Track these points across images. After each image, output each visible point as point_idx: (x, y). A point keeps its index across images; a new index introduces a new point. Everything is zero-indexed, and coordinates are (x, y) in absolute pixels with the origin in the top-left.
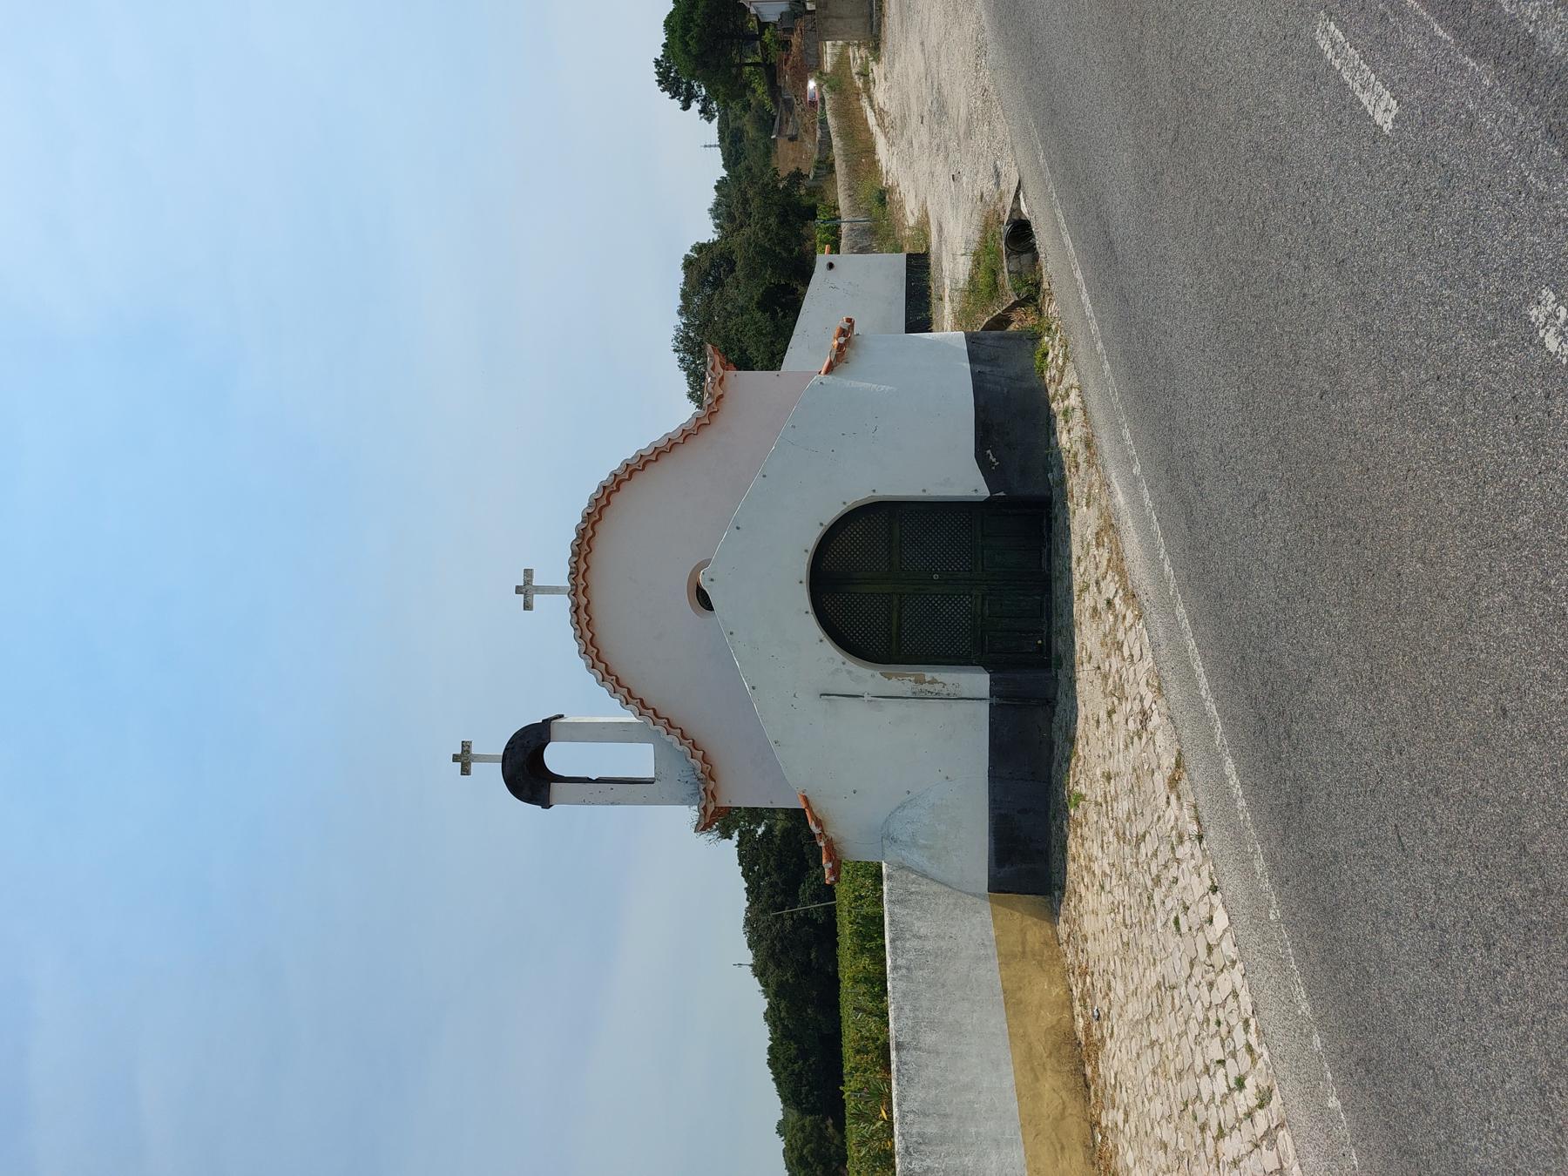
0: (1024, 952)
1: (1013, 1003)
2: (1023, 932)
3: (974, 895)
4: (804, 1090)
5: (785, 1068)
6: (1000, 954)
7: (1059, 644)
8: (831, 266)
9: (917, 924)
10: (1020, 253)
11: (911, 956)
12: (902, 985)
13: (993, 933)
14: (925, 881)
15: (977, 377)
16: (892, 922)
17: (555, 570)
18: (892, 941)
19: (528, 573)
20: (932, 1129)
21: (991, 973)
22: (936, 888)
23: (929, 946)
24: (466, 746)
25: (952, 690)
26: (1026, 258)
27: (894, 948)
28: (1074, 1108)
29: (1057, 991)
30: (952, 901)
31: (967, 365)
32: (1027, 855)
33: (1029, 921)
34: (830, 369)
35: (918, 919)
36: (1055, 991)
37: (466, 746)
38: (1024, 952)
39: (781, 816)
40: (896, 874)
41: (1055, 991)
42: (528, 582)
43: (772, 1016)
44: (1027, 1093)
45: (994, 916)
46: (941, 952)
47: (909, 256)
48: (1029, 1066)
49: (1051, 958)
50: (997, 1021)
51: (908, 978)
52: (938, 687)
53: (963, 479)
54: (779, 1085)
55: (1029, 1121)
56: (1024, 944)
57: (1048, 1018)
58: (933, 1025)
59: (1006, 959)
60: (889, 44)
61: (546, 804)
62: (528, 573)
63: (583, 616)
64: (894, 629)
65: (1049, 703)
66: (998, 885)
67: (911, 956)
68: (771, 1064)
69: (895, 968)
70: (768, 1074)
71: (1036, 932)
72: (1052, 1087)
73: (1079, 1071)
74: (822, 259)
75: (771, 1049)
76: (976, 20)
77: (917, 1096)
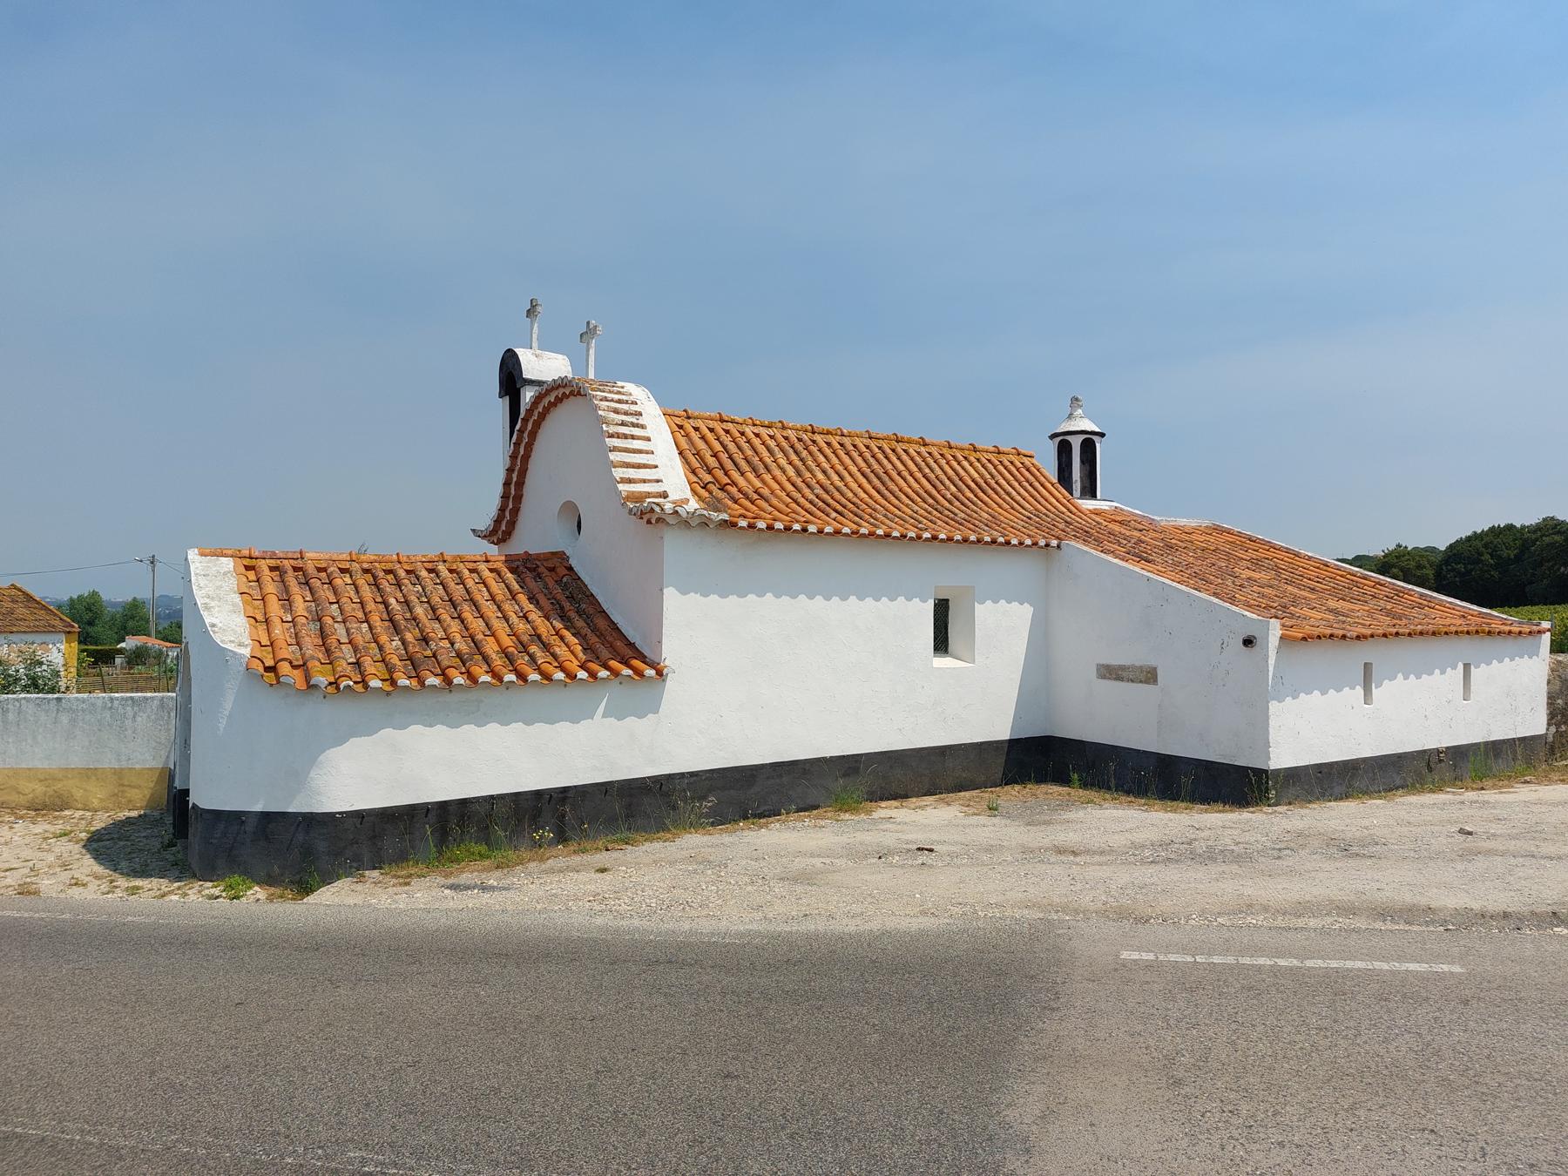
1: (88, 774)
2: (139, 787)
4: (1461, 567)
5: (1486, 546)
8: (1248, 642)
11: (121, 710)
12: (99, 703)
15: (237, 817)
16: (146, 698)
20: (11, 716)
21: (109, 762)
23: (128, 723)
27: (127, 699)
28: (22, 800)
29: (96, 803)
33: (147, 793)
34: (941, 644)
36: (96, 802)
41: (96, 802)
44: (32, 774)
48: (47, 778)
50: (77, 762)
51: (104, 707)
54: (1469, 539)
55: (16, 773)
57: (78, 794)
58: (73, 721)
59: (118, 773)
60: (1303, 811)
67: (121, 710)
68: (1492, 529)
69: (112, 699)
70: (1482, 526)
72: (37, 790)
73: (45, 807)
75: (1510, 527)
77: (30, 709)
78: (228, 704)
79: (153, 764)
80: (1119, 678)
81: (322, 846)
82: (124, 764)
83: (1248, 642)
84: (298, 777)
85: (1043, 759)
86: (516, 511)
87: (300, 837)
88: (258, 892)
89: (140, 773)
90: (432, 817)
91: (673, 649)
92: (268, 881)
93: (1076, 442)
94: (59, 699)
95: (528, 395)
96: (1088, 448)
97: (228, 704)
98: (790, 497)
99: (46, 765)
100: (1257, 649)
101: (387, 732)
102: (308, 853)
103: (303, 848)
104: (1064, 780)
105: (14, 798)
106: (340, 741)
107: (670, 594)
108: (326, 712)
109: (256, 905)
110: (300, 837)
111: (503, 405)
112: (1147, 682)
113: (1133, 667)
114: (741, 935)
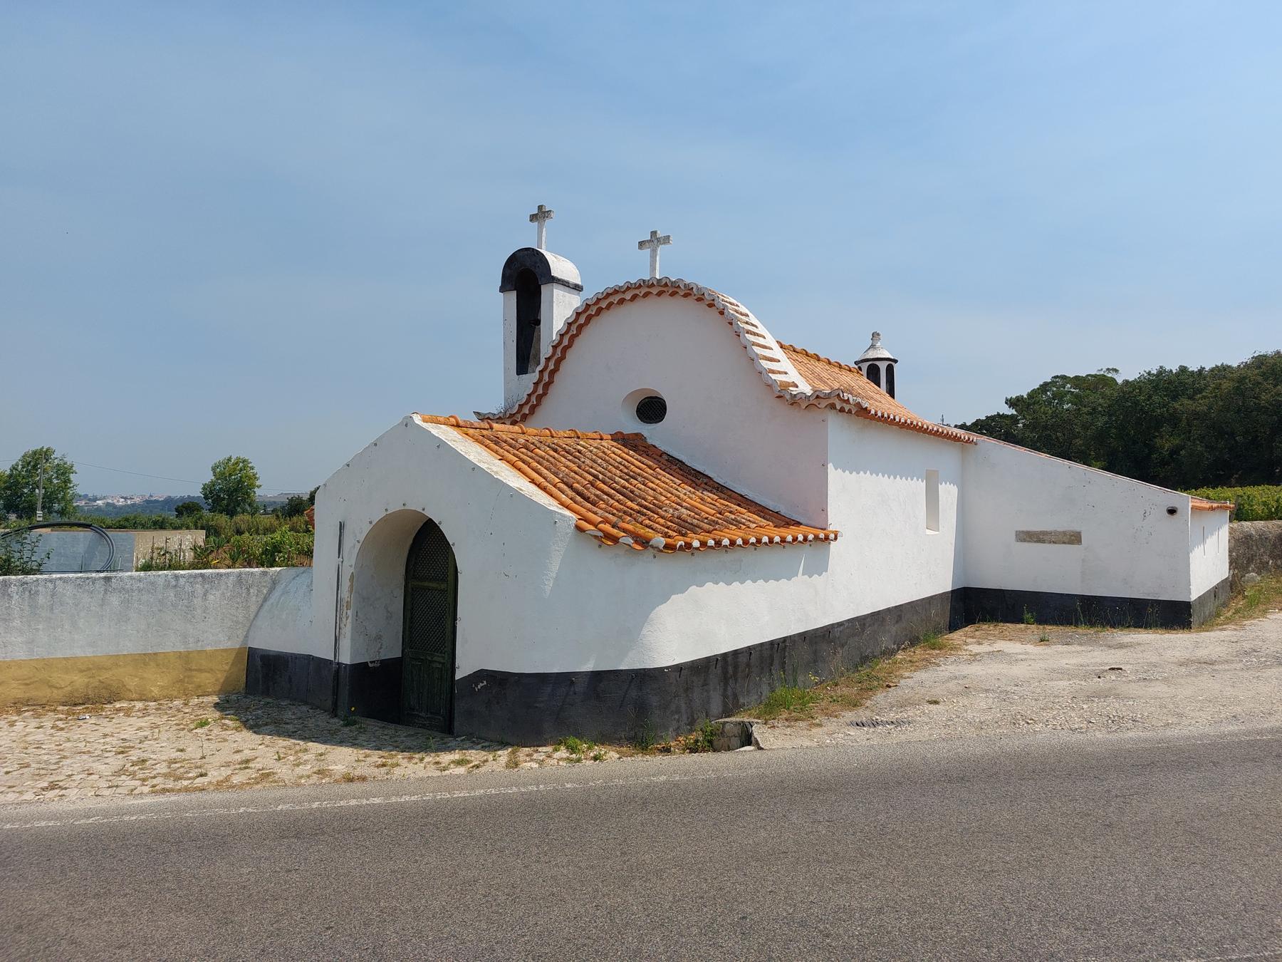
0: (190, 670)
2: (211, 671)
3: (246, 636)
8: (1172, 511)
12: (161, 581)
13: (208, 648)
14: (260, 600)
15: (566, 679)
17: (665, 266)
18: (202, 575)
19: (667, 239)
20: (41, 600)
21: (172, 644)
22: (254, 608)
23: (197, 602)
25: (343, 631)
27: (196, 576)
28: (57, 694)
29: (156, 691)
30: (241, 619)
31: (589, 667)
33: (221, 677)
38: (190, 670)
40: (268, 578)
42: (658, 240)
44: (70, 664)
46: (227, 612)
48: (90, 667)
50: (129, 647)
55: (48, 664)
56: (200, 670)
57: (132, 683)
59: (185, 658)
61: (502, 289)
62: (667, 239)
63: (616, 298)
64: (426, 584)
66: (252, 652)
67: (188, 588)
69: (176, 577)
72: (79, 681)
73: (86, 700)
77: (69, 590)
78: (555, 566)
79: (228, 645)
80: (1040, 541)
81: (654, 700)
82: (192, 647)
83: (1172, 511)
84: (631, 633)
85: (974, 606)
86: (540, 398)
87: (633, 693)
88: (612, 754)
89: (211, 655)
90: (716, 672)
91: (835, 521)
92: (605, 739)
93: (883, 367)
94: (108, 579)
95: (560, 309)
96: (890, 370)
97: (555, 566)
98: (862, 401)
99: (89, 652)
100: (1175, 516)
101: (693, 589)
102: (642, 709)
103: (624, 705)
104: (1020, 620)
105: (43, 693)
106: (665, 599)
107: (830, 466)
108: (654, 569)
109: (614, 766)
110: (633, 693)
111: (500, 309)
112: (1071, 542)
113: (1055, 532)
114: (105, 813)
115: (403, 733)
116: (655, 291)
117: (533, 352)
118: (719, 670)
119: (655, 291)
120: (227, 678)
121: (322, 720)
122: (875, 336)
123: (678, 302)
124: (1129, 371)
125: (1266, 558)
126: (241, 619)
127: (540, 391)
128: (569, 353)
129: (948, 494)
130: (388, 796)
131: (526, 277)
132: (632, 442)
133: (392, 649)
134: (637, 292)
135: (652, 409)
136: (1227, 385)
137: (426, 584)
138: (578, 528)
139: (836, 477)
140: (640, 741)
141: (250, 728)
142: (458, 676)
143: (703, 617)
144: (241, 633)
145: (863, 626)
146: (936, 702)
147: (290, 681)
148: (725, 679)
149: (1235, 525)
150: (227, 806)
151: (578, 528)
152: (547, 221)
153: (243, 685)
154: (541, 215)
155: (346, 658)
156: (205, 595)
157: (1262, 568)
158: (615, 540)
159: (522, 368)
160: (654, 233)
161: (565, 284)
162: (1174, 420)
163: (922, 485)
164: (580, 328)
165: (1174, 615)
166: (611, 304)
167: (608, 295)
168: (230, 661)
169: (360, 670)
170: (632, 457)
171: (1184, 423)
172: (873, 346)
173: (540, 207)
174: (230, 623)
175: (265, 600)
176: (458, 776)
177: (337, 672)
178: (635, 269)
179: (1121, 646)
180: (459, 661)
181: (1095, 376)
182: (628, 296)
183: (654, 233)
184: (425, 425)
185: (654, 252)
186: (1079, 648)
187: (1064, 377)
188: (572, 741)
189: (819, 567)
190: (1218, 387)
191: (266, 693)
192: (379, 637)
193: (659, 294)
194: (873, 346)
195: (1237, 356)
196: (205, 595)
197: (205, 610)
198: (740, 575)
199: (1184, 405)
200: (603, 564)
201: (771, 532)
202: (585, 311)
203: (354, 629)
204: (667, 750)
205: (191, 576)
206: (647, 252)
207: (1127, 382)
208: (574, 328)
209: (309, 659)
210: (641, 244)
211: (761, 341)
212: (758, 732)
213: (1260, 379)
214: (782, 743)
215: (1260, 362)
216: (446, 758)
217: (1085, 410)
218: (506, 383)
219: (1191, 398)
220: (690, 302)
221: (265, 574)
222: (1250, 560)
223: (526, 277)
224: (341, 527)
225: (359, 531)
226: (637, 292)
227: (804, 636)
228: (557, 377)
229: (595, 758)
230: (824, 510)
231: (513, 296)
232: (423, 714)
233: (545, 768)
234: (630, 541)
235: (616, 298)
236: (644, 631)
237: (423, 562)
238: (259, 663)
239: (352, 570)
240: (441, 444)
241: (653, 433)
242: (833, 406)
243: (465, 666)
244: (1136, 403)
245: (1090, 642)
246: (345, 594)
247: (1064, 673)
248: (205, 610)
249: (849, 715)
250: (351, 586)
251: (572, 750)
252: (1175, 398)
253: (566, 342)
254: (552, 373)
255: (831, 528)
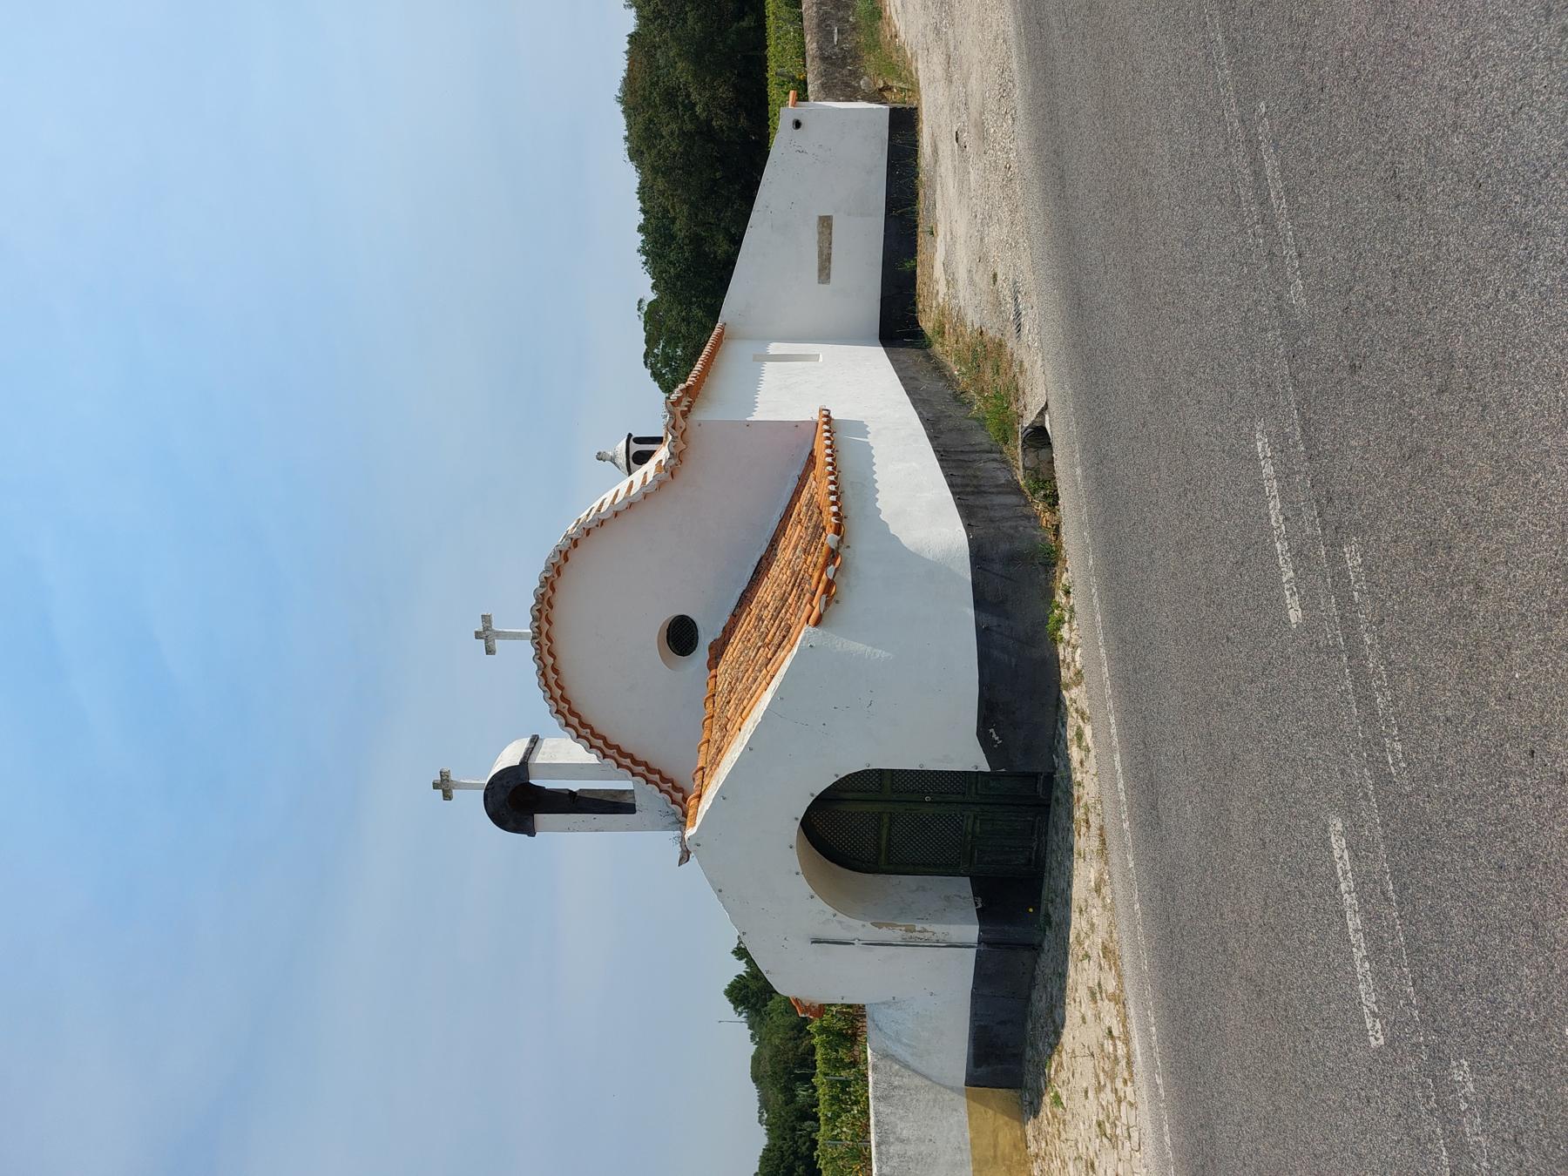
0: (995, 1157)
3: (952, 1089)
6: (974, 1160)
7: (1039, 1003)
8: (798, 124)
9: (901, 1125)
10: (1038, 448)
13: (968, 1135)
14: (907, 1073)
15: (983, 634)
16: (878, 1122)
17: (517, 617)
18: (878, 1145)
19: (486, 619)
22: (918, 1081)
23: (911, 1150)
24: (445, 776)
25: (941, 937)
26: (1043, 453)
27: (879, 1153)
30: (931, 1096)
31: (971, 612)
32: (1009, 1052)
33: (1002, 1120)
35: (901, 1119)
37: (445, 776)
38: (995, 1157)
39: (723, 248)
40: (881, 1064)
42: (486, 629)
43: (644, 192)
45: (970, 1115)
47: (893, 111)
49: (1019, 1162)
52: (927, 935)
53: (961, 752)
56: (995, 1146)
61: (532, 833)
62: (486, 619)
63: (551, 675)
64: (884, 842)
65: (1036, 948)
66: (973, 1081)
71: (1006, 1132)
74: (785, 112)
76: (1005, 20)
78: (859, 647)
79: (962, 1114)
80: (829, 259)
81: (1004, 547)
83: (798, 124)
85: (899, 324)
86: (664, 780)
89: (977, 1131)
90: (971, 500)
93: (635, 448)
96: (639, 441)
97: (859, 647)
102: (1013, 558)
103: (1010, 582)
106: (895, 539)
108: (861, 548)
110: (997, 567)
111: (559, 838)
112: (830, 227)
115: (1052, 862)
116: (546, 627)
117: (608, 799)
118: (971, 498)
119: (546, 627)
120: (1004, 1112)
121: (1046, 963)
122: (600, 457)
123: (560, 600)
124: (642, 286)
125: (845, 72)
126: (931, 1096)
127: (656, 777)
128: (613, 741)
129: (774, 348)
130: (1113, 751)
131: (517, 801)
132: (718, 650)
133: (962, 886)
134: (545, 649)
135: (681, 636)
136: (661, 184)
137: (884, 842)
138: (817, 623)
139: (759, 415)
140: (1049, 560)
141: (1058, 1035)
142: (985, 767)
143: (915, 506)
144: (948, 1095)
145: (924, 401)
146: (995, 276)
147: (1003, 1023)
148: (979, 491)
149: (811, 98)
150: (1145, 1031)
151: (817, 623)
152: (452, 778)
153: (1012, 1092)
154: (445, 786)
155: (972, 932)
156: (902, 1141)
157: (855, 74)
158: (830, 584)
159: (630, 809)
160: (478, 635)
161: (529, 752)
162: (696, 241)
163: (768, 366)
164: (583, 725)
165: (904, 124)
166: (555, 671)
167: (546, 685)
168: (982, 1109)
169: (983, 916)
170: (731, 652)
171: (698, 230)
172: (613, 460)
173: (436, 786)
174: (937, 1110)
175: (906, 1066)
176: (1094, 735)
177: (988, 944)
178: (520, 657)
179: (935, 151)
180: (969, 768)
181: (646, 323)
182: (550, 661)
183: (478, 635)
184: (698, 822)
185: (499, 635)
186: (938, 192)
187: (646, 356)
188: (1050, 627)
189: (860, 428)
190: (662, 193)
191: (1019, 1058)
192: (947, 898)
193: (549, 622)
194: (613, 460)
195: (630, 177)
196: (902, 1141)
197: (920, 1140)
198: (868, 487)
199: (680, 228)
200: (858, 597)
201: (819, 486)
202: (564, 716)
203: (938, 922)
204: (1057, 530)
205: (879, 1159)
206: (498, 644)
207: (654, 287)
208: (583, 732)
209: (976, 995)
210: (490, 651)
211: (609, 500)
212: (1029, 419)
213: (654, 152)
214: (1041, 388)
215: (635, 154)
216: (1075, 753)
217: (684, 329)
218: (643, 828)
219: (673, 221)
220: (567, 570)
221: (875, 1068)
222: (848, 85)
223: (517, 801)
224: (816, 941)
225: (818, 913)
226: (545, 649)
227: (933, 438)
228: (640, 757)
229: (1067, 593)
230: (797, 425)
231: (541, 819)
232: (1034, 845)
233: (1081, 646)
234: (831, 568)
235: (551, 675)
236: (930, 557)
237: (861, 830)
238: (982, 1070)
239: (868, 924)
240: (722, 795)
241: (707, 635)
242: (684, 415)
243: (973, 759)
244: (678, 277)
245: (932, 180)
246: (895, 934)
247: (962, 182)
248: (920, 1140)
249: (1011, 344)
250: (887, 925)
251: (1061, 621)
252: (673, 237)
253: (600, 743)
254: (635, 762)
255: (816, 417)
